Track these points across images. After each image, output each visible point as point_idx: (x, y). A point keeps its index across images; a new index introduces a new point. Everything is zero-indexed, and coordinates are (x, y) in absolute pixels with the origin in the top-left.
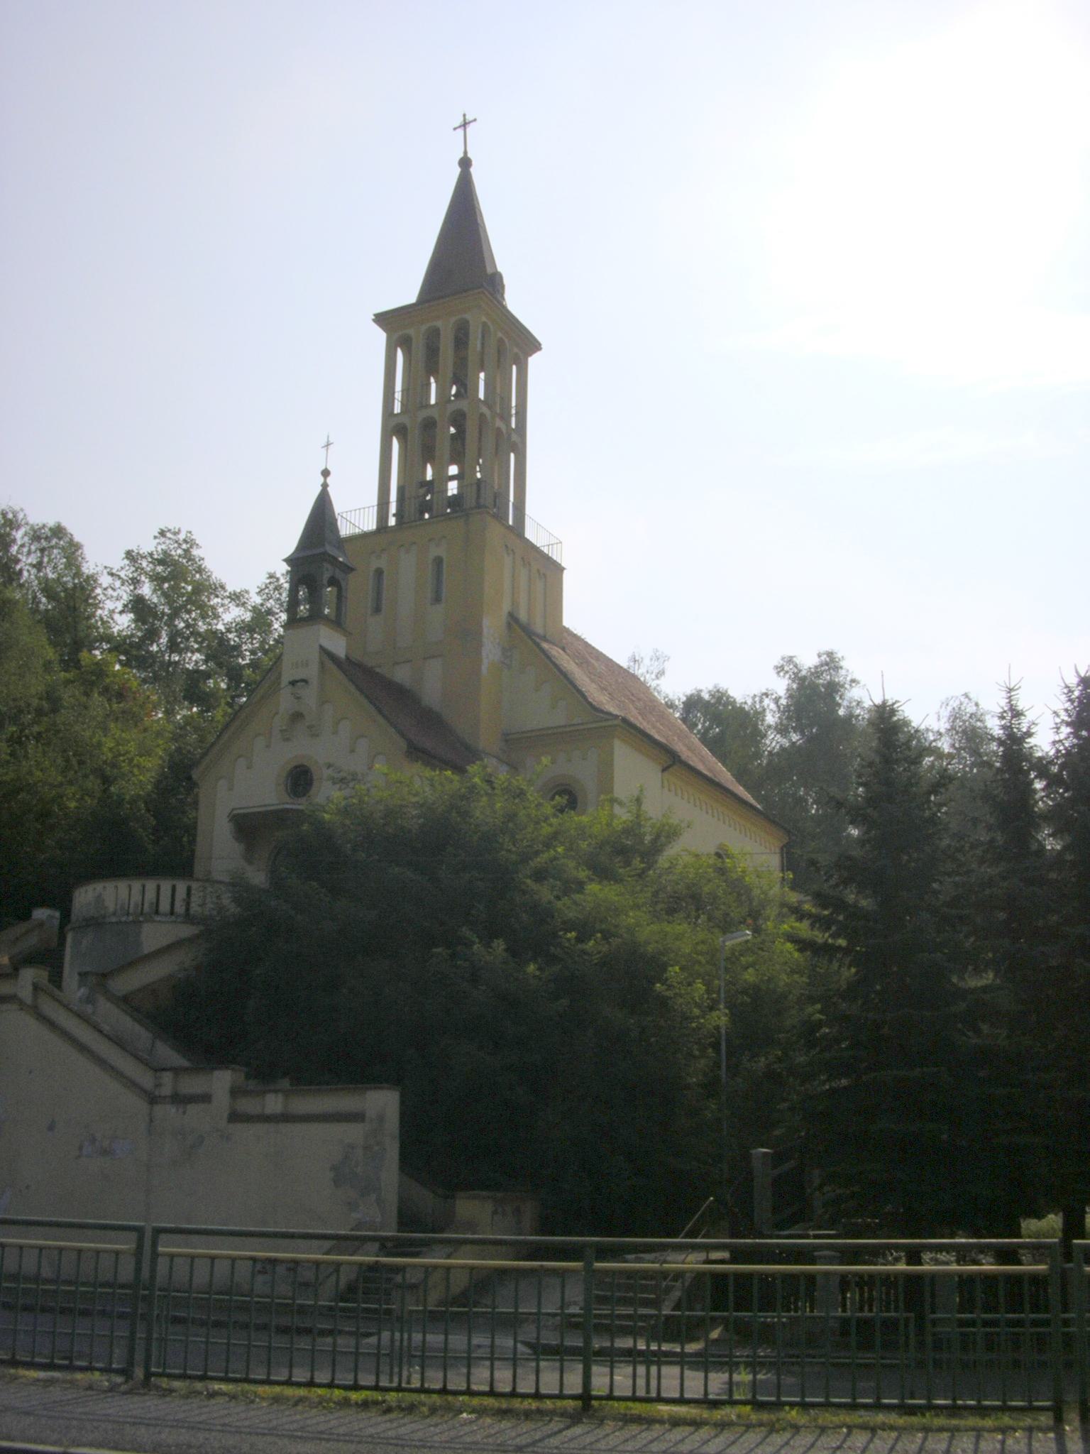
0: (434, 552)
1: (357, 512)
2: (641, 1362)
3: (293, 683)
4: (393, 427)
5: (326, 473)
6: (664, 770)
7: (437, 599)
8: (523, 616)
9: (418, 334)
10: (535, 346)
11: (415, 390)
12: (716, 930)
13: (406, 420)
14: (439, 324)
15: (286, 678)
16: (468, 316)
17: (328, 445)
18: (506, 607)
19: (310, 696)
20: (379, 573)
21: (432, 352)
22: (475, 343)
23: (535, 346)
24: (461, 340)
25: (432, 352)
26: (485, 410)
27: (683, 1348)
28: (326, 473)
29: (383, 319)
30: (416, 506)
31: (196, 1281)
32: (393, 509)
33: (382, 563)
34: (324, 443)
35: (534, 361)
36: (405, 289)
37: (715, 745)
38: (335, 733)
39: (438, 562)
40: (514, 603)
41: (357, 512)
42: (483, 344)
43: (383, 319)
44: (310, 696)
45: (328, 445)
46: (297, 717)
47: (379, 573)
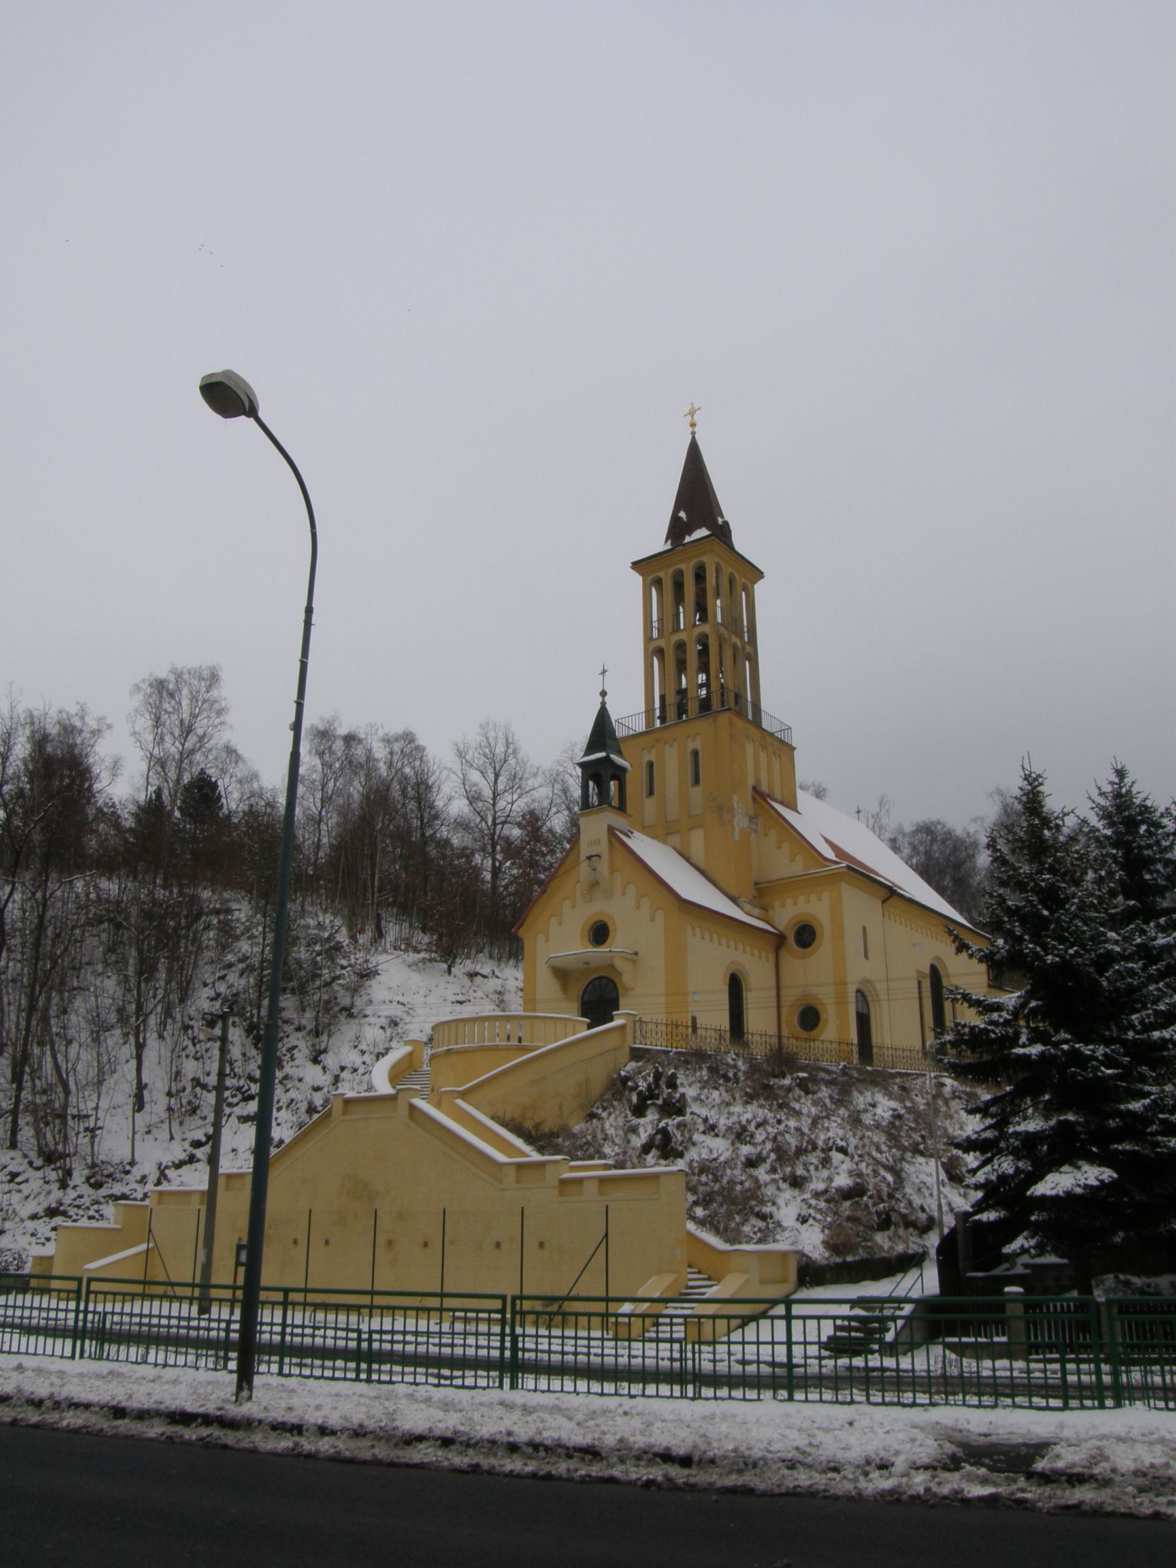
0: (692, 745)
1: (630, 711)
2: (906, 1371)
3: (589, 858)
4: (654, 651)
5: (603, 694)
6: (883, 902)
7: (696, 781)
8: (764, 788)
9: (667, 576)
10: (758, 574)
11: (669, 623)
12: (784, 1186)
13: (662, 643)
14: (682, 566)
15: (583, 856)
16: (704, 559)
17: (604, 672)
18: (751, 782)
19: (603, 867)
20: (651, 765)
21: (679, 585)
22: (711, 580)
23: (758, 574)
24: (700, 576)
25: (679, 585)
26: (722, 630)
27: (1079, 1378)
28: (603, 694)
29: (636, 565)
30: (675, 708)
31: (158, 1303)
32: (655, 618)
33: (652, 757)
34: (601, 670)
35: (759, 588)
36: (654, 539)
37: (928, 872)
38: (624, 894)
39: (695, 753)
40: (758, 780)
41: (630, 711)
42: (717, 578)
43: (636, 565)
44: (603, 867)
45: (604, 672)
46: (595, 884)
47: (651, 765)
